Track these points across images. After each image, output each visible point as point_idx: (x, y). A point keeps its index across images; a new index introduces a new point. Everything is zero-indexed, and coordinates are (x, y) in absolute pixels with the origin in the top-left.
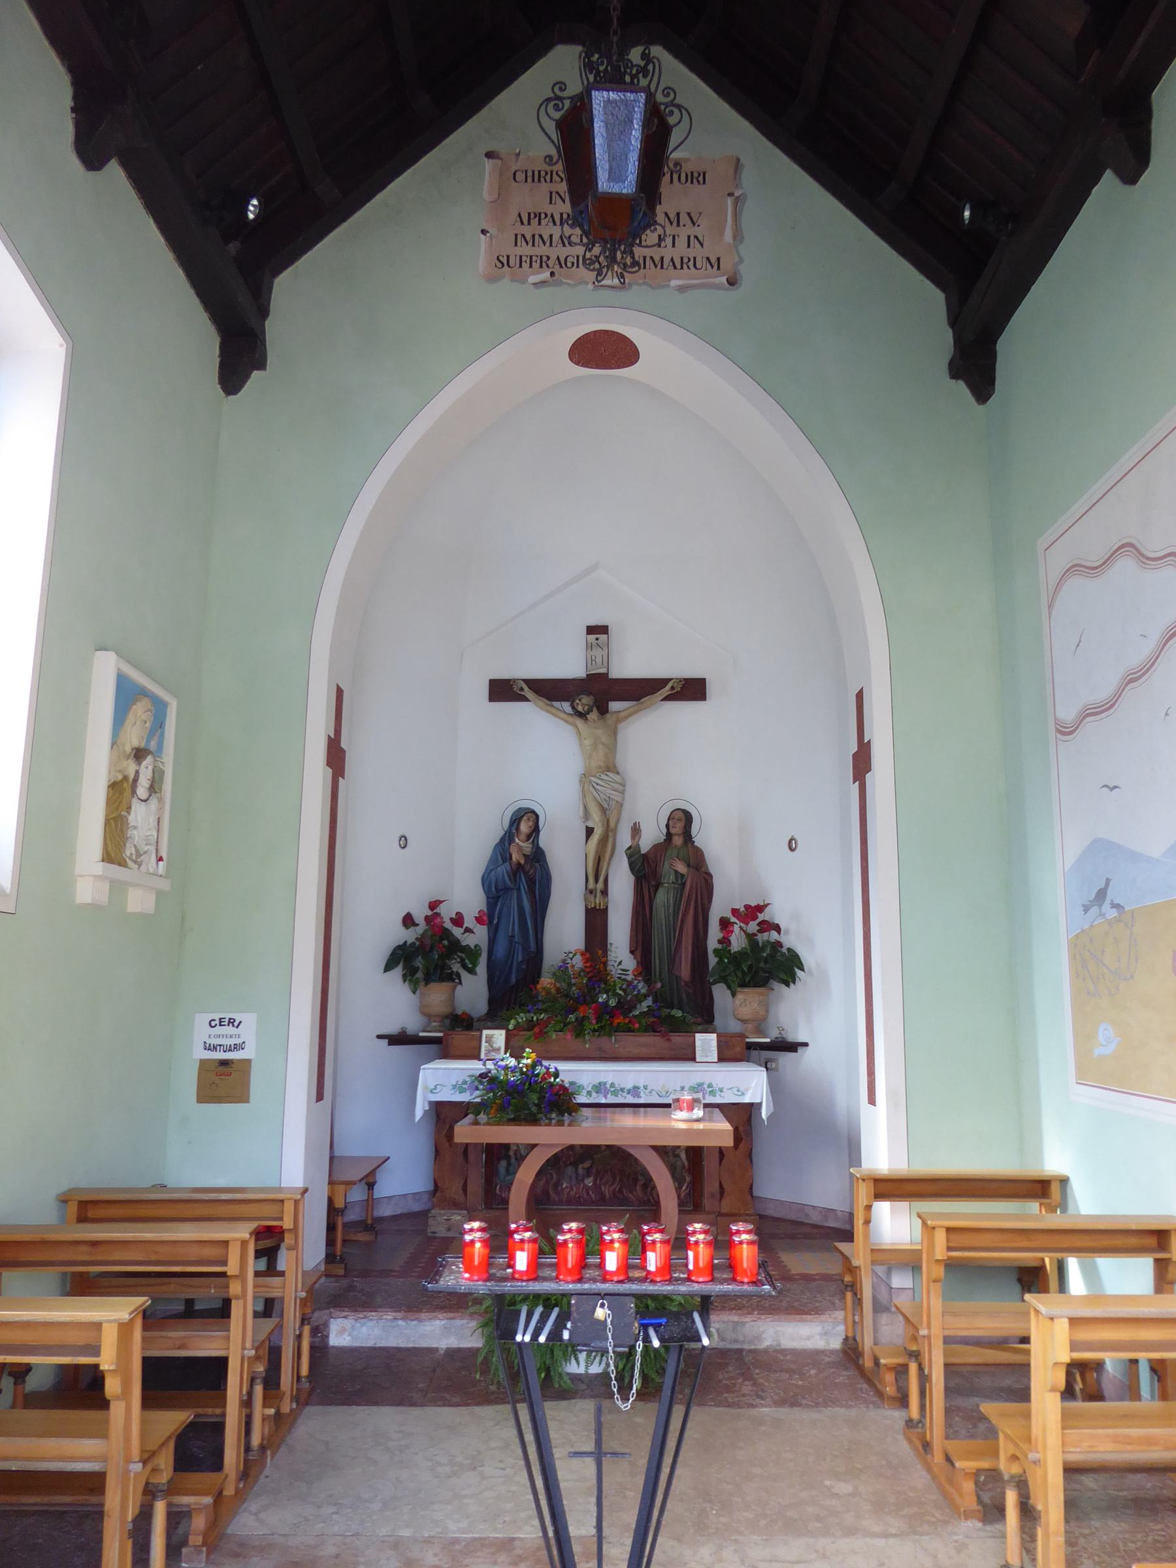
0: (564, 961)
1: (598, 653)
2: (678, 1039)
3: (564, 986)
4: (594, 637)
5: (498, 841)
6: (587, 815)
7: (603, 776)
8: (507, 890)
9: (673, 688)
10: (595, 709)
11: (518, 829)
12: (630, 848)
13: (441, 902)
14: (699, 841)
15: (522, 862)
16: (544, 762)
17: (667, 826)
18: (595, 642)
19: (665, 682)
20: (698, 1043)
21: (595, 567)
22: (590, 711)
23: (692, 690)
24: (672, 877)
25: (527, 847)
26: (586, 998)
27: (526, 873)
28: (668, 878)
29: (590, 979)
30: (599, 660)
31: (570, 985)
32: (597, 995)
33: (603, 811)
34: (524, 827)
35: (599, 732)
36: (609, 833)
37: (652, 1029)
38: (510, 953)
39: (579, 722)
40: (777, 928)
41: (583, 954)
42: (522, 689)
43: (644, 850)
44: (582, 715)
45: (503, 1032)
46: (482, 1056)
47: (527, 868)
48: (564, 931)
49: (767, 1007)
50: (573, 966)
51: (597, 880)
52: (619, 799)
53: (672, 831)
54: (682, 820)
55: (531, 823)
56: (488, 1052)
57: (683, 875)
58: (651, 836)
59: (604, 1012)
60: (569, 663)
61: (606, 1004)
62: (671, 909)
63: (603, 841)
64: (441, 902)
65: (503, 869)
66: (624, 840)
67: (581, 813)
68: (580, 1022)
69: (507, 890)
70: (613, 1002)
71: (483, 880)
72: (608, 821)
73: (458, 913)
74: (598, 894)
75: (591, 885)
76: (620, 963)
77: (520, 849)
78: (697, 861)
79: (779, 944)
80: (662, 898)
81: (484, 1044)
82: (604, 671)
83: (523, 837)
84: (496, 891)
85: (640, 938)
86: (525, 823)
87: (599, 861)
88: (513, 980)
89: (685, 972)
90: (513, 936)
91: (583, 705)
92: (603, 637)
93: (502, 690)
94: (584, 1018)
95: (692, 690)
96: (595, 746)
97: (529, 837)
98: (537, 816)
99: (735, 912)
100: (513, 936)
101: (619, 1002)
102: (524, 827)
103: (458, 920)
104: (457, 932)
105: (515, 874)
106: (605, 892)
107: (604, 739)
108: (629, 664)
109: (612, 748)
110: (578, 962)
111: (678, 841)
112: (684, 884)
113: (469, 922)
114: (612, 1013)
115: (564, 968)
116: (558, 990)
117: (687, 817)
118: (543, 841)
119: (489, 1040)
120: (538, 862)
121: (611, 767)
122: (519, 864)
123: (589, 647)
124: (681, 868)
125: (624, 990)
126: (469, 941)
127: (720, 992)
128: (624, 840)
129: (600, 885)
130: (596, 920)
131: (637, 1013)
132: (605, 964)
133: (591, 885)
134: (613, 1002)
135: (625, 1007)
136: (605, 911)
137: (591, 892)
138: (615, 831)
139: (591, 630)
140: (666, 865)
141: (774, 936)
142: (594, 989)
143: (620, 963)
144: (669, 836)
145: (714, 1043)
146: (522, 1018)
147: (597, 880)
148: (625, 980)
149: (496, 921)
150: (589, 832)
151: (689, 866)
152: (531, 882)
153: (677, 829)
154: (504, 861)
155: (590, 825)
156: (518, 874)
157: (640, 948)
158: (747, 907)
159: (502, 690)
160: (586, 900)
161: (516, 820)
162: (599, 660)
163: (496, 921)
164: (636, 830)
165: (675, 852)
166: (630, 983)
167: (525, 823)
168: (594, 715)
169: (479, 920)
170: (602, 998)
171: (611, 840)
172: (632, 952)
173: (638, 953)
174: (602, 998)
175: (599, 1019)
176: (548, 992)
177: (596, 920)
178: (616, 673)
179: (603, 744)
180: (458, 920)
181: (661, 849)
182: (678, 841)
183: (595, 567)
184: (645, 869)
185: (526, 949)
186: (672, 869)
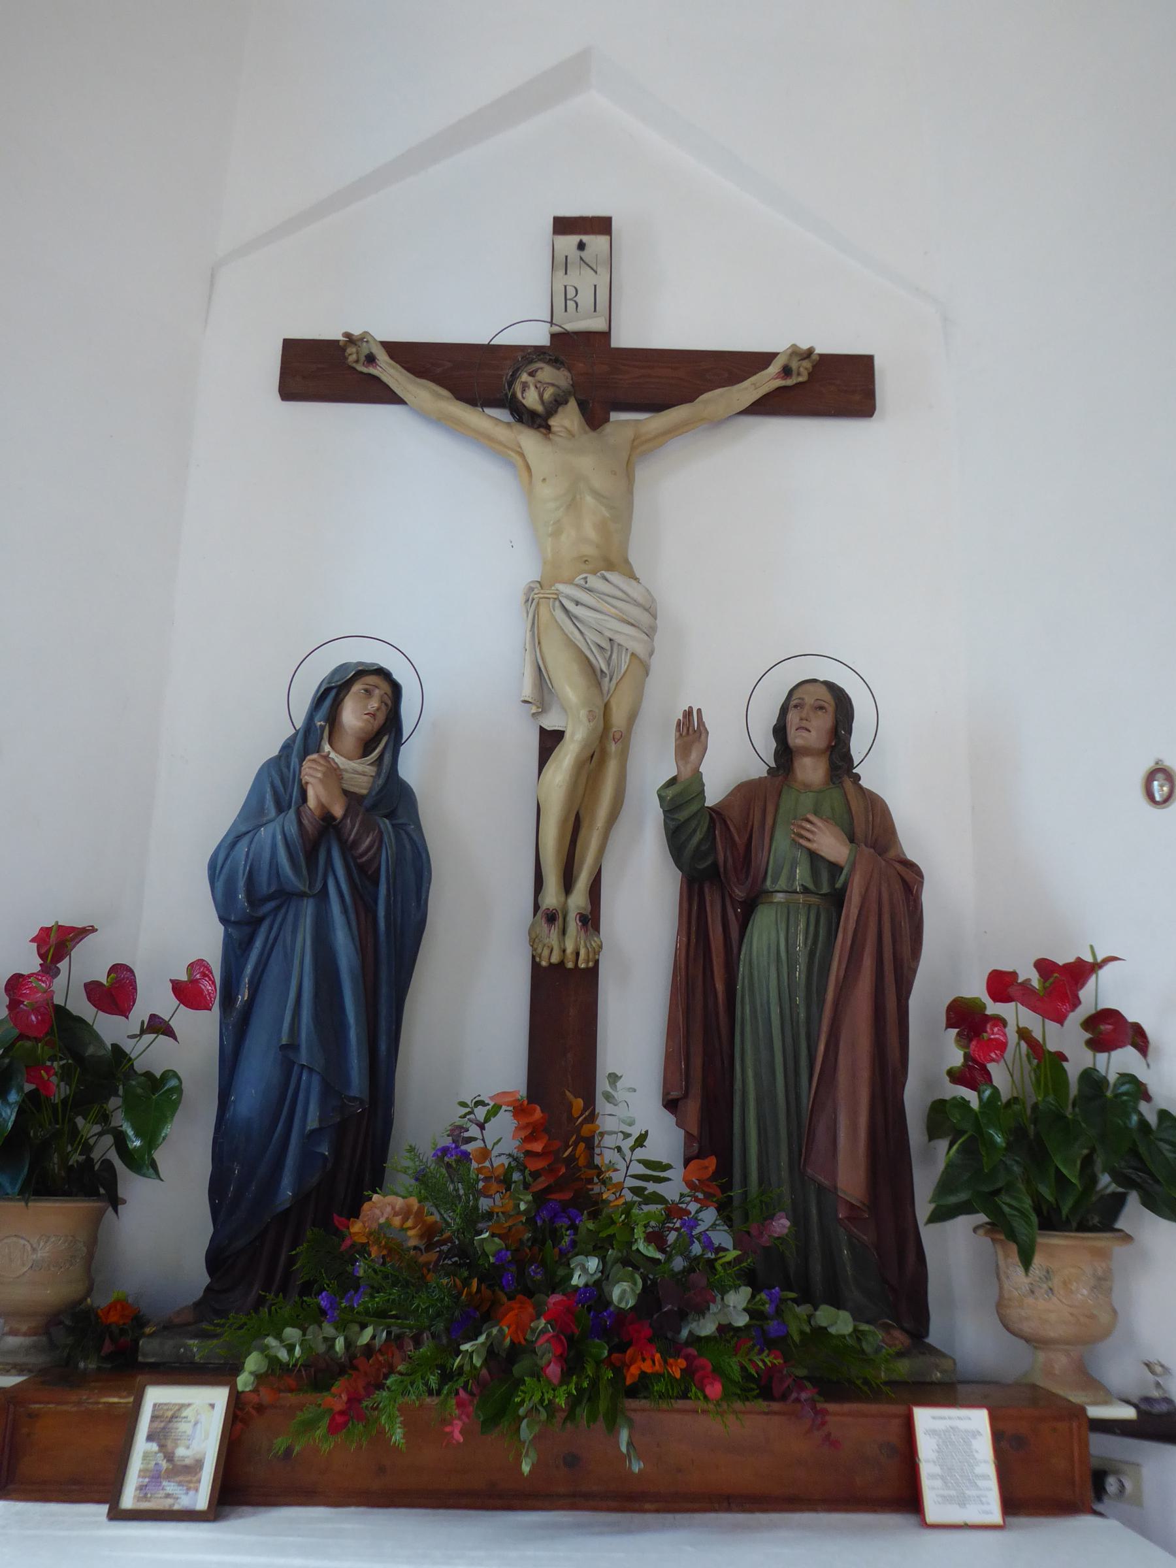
0: (458, 1134)
1: (583, 280)
2: (853, 1424)
3: (454, 1220)
4: (574, 240)
5: (275, 752)
6: (543, 691)
7: (594, 582)
8: (284, 896)
9: (786, 371)
10: (572, 404)
11: (333, 719)
12: (673, 782)
13: (81, 933)
14: (870, 775)
15: (338, 811)
16: (430, 566)
17: (780, 731)
18: (574, 253)
19: (758, 361)
20: (926, 1447)
21: (572, 75)
22: (555, 405)
23: (835, 387)
24: (802, 874)
25: (360, 773)
26: (530, 1267)
27: (348, 849)
28: (786, 876)
29: (540, 1198)
30: (585, 299)
31: (473, 1219)
32: (564, 1259)
33: (594, 676)
34: (354, 716)
35: (586, 463)
36: (606, 748)
37: (763, 1387)
38: (283, 1101)
39: (529, 440)
40: (1139, 1038)
41: (519, 1110)
42: (371, 359)
43: (714, 794)
44: (537, 421)
45: (219, 1396)
46: (128, 1500)
47: (352, 830)
48: (466, 1035)
49: (1103, 1284)
50: (485, 1154)
51: (568, 884)
52: (640, 649)
53: (796, 739)
54: (819, 728)
55: (374, 704)
56: (154, 1477)
57: (835, 869)
58: (731, 761)
59: (591, 1329)
60: (503, 303)
61: (596, 1293)
62: (800, 973)
63: (593, 763)
64: (81, 933)
65: (274, 834)
66: (652, 765)
67: (527, 691)
68: (504, 1361)
69: (284, 896)
70: (623, 1293)
71: (214, 870)
72: (607, 706)
73: (116, 969)
74: (573, 926)
75: (552, 897)
76: (641, 1141)
77: (333, 773)
78: (871, 825)
79: (1140, 1091)
80: (771, 940)
81: (142, 1446)
82: (596, 324)
83: (349, 742)
84: (250, 899)
85: (697, 1062)
86: (361, 706)
87: (575, 828)
88: (287, 1192)
89: (850, 1177)
90: (292, 1047)
91: (540, 387)
92: (596, 243)
93: (319, 371)
94: (516, 1352)
95: (835, 387)
96: (572, 504)
97: (367, 746)
98: (396, 689)
99: (1002, 985)
100: (292, 1047)
101: (649, 1297)
102: (354, 716)
103: (116, 992)
104: (111, 1029)
105: (311, 854)
106: (591, 920)
107: (599, 481)
108: (662, 316)
109: (620, 512)
110: (502, 1137)
111: (811, 770)
112: (837, 899)
113: (155, 997)
114: (618, 1330)
115: (455, 1154)
116: (430, 1233)
117: (841, 707)
118: (412, 766)
119: (166, 1421)
120: (390, 815)
121: (612, 559)
122: (327, 818)
123: (560, 265)
124: (831, 845)
125: (656, 1238)
126: (153, 1055)
127: (954, 1249)
128: (652, 765)
129: (578, 899)
130: (563, 1002)
131: (707, 1327)
132: (590, 1144)
133: (552, 897)
134: (623, 1293)
135: (671, 1299)
136: (590, 976)
137: (551, 918)
138: (624, 739)
139: (563, 226)
140: (781, 843)
141: (1121, 1061)
142: (556, 1237)
143: (641, 1141)
144: (785, 755)
145: (983, 1448)
146: (288, 1345)
147: (568, 884)
148: (657, 1198)
149: (243, 996)
150: (550, 741)
151: (852, 839)
152: (364, 877)
153: (811, 734)
154: (281, 808)
155: (552, 722)
156: (333, 854)
157: (696, 1089)
158: (1044, 967)
159: (319, 371)
160: (533, 941)
161: (331, 695)
162: (585, 299)
163: (243, 996)
164: (691, 732)
165: (807, 800)
166: (673, 1211)
167: (361, 706)
168: (568, 419)
169: (188, 993)
170: (585, 1270)
171: (612, 767)
172: (671, 1105)
173: (693, 1107)
174: (585, 1270)
175: (572, 1364)
176: (393, 1250)
177: (563, 1002)
178: (629, 335)
179: (596, 494)
180: (116, 992)
181: (759, 798)
182: (811, 770)
183: (572, 75)
184: (717, 852)
185: (332, 1089)
186: (789, 859)
